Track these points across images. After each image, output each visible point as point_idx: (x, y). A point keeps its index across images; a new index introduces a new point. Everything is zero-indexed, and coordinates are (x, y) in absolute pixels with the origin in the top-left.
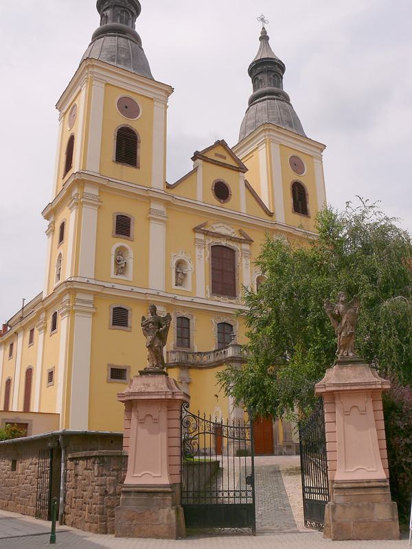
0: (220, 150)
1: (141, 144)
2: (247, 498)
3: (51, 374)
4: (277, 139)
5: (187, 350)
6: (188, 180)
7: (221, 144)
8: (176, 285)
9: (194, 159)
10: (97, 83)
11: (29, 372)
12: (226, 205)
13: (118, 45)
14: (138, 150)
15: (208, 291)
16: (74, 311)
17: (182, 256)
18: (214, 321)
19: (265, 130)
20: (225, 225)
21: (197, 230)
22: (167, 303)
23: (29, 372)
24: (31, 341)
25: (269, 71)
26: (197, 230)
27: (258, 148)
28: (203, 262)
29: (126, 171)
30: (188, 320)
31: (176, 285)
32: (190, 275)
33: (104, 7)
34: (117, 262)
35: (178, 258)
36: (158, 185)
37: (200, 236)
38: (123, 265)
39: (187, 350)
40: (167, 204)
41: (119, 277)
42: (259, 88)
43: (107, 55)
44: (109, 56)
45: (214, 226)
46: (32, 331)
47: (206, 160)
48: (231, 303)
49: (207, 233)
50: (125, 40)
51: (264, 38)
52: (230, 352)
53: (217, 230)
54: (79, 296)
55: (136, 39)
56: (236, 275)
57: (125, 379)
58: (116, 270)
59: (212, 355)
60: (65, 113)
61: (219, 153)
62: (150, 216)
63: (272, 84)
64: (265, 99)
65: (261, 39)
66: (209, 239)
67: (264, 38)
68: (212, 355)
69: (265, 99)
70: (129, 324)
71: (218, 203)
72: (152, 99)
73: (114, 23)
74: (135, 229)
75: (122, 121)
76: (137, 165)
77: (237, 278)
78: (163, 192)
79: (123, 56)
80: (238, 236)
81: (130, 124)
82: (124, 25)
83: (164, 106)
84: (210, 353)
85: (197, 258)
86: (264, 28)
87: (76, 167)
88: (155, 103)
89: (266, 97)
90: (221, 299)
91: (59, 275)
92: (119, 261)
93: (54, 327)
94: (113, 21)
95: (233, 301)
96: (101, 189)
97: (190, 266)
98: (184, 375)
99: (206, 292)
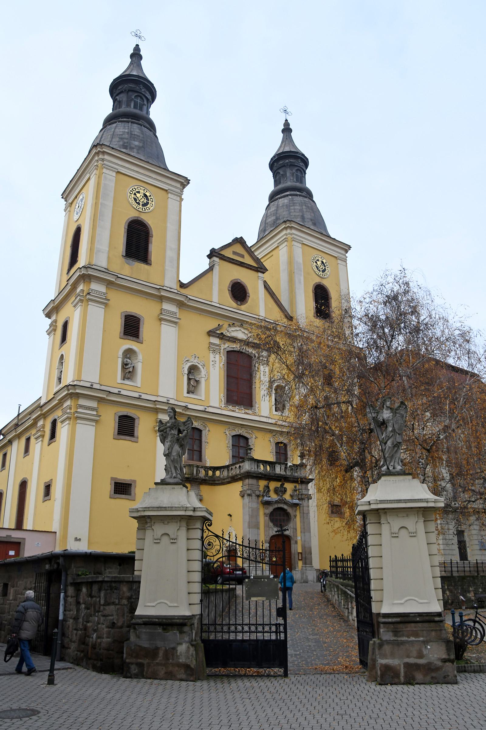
0: (238, 248)
1: (153, 238)
2: (229, 633)
3: (48, 488)
5: (198, 463)
6: (203, 279)
7: (240, 241)
9: (210, 256)
11: (23, 485)
12: (243, 307)
14: (150, 245)
15: (223, 400)
17: (195, 362)
21: (211, 333)
23: (23, 485)
24: (27, 450)
25: (292, 165)
26: (211, 333)
27: (278, 247)
28: (217, 365)
31: (188, 393)
33: (118, 92)
34: (125, 365)
35: (192, 363)
36: (170, 283)
37: (216, 341)
38: (131, 370)
39: (198, 463)
41: (127, 382)
44: (121, 143)
46: (28, 440)
48: (247, 414)
49: (222, 337)
50: (139, 126)
53: (234, 334)
54: (82, 402)
61: (238, 251)
63: (295, 180)
64: (287, 195)
66: (224, 344)
69: (287, 195)
70: (136, 434)
71: (234, 304)
72: (166, 191)
74: (145, 330)
76: (149, 262)
77: (254, 387)
78: (176, 291)
79: (137, 143)
82: (137, 111)
84: (224, 467)
85: (212, 363)
86: (286, 120)
87: (82, 261)
88: (170, 195)
89: (288, 193)
90: (236, 408)
91: (60, 379)
92: (126, 365)
93: (53, 435)
95: (250, 412)
96: (108, 286)
97: (203, 372)
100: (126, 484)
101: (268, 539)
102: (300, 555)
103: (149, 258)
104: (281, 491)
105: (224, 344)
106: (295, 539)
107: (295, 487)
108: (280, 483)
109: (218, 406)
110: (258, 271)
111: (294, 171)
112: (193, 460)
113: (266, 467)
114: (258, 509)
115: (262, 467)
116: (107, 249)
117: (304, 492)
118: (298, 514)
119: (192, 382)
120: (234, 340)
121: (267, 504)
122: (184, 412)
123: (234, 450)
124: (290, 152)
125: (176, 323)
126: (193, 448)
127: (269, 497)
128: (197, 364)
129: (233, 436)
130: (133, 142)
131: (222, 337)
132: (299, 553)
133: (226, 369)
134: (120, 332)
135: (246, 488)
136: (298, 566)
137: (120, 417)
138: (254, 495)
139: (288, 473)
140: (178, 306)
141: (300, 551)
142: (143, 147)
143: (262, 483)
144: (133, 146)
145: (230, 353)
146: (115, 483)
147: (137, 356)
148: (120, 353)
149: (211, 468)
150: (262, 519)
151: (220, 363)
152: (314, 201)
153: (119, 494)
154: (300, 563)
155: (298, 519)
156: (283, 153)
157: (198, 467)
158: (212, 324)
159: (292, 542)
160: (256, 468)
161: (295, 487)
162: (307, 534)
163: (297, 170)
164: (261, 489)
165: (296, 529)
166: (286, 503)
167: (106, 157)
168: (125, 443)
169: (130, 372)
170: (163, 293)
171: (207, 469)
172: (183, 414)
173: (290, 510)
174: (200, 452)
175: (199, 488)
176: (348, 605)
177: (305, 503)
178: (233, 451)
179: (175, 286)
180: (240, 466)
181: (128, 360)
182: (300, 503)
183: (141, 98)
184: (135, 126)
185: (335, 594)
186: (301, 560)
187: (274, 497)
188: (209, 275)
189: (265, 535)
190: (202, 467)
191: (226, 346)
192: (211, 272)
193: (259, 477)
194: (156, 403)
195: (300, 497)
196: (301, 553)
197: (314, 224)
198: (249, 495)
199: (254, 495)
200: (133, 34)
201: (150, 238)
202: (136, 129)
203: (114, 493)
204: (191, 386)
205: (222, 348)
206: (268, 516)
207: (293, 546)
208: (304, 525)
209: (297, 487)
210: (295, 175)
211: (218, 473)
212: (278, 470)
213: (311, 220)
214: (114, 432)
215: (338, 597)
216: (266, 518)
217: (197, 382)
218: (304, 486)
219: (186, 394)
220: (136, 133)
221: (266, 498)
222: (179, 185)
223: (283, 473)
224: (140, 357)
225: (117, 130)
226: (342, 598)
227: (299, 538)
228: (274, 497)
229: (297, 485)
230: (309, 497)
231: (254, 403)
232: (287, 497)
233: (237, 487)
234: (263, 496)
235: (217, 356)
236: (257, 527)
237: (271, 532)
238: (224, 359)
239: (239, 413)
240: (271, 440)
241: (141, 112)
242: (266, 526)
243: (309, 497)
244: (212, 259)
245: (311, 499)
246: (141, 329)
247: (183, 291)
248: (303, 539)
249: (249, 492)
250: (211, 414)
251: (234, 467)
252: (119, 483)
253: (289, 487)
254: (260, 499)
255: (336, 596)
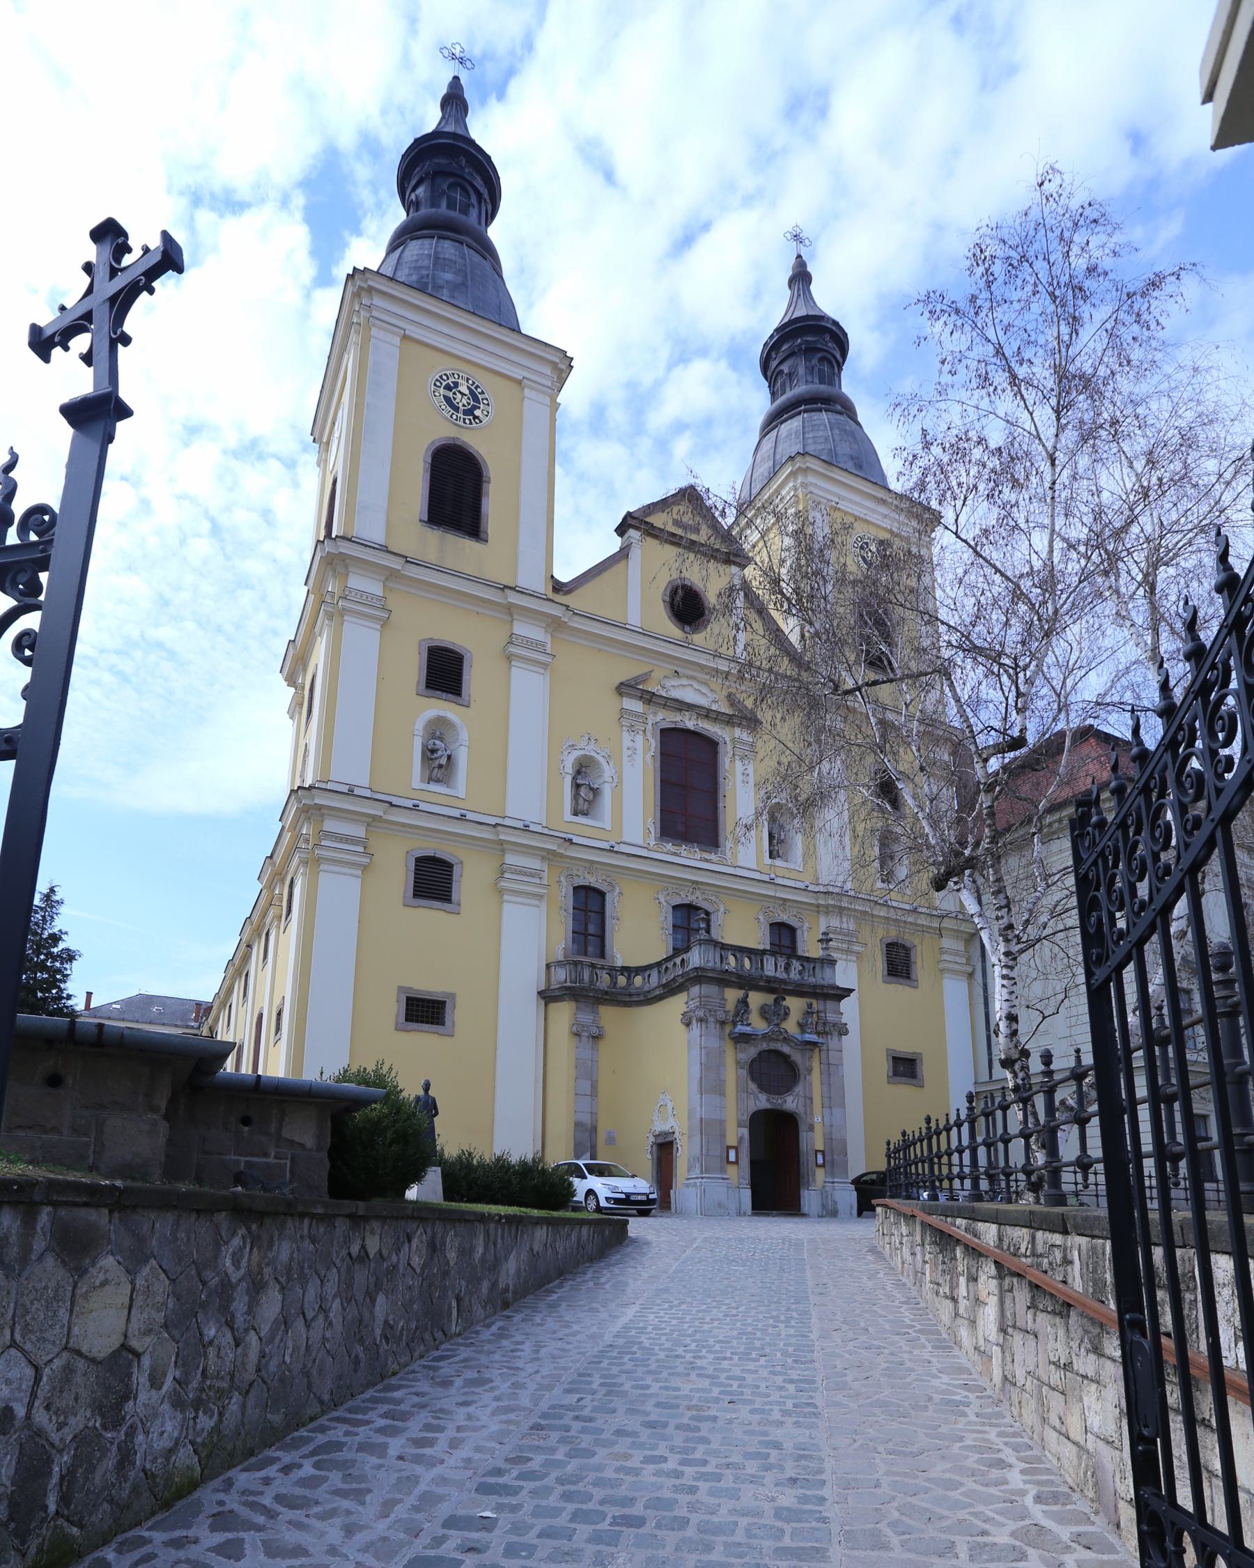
0: (683, 511)
4: (822, 494)
5: (600, 962)
6: (606, 576)
7: (690, 496)
8: (576, 814)
9: (621, 530)
10: (382, 335)
12: (698, 638)
13: (436, 252)
14: (484, 500)
15: (652, 830)
16: (319, 860)
17: (590, 750)
18: (668, 900)
19: (793, 474)
20: (696, 685)
21: (625, 689)
22: (549, 851)
25: (809, 351)
26: (625, 689)
28: (639, 758)
29: (459, 549)
30: (602, 894)
32: (607, 791)
33: (413, 182)
34: (429, 753)
35: (582, 752)
36: (529, 577)
37: (636, 706)
38: (443, 761)
39: (600, 962)
40: (555, 625)
41: (433, 787)
42: (783, 393)
43: (411, 275)
45: (668, 683)
47: (651, 532)
48: (707, 861)
49: (649, 698)
51: (801, 278)
52: (695, 958)
53: (675, 694)
54: (330, 825)
55: (487, 251)
56: (721, 796)
57: (443, 1024)
58: (427, 772)
59: (654, 973)
60: (328, 443)
62: (512, 649)
63: (817, 380)
64: (799, 413)
65: (792, 282)
66: (655, 714)
67: (801, 278)
68: (654, 973)
70: (454, 897)
71: (673, 630)
72: (519, 382)
73: (433, 210)
74: (475, 678)
75: (443, 429)
76: (482, 535)
77: (721, 805)
79: (449, 276)
80: (725, 708)
81: (465, 439)
82: (455, 214)
83: (547, 400)
84: (649, 967)
85: (626, 753)
86: (799, 256)
90: (683, 849)
92: (433, 751)
94: (433, 206)
95: (713, 857)
96: (391, 584)
97: (608, 771)
98: (586, 1017)
99: (814, 1174)
100: (434, 1002)
101: (746, 1118)
102: (820, 1157)
103: (482, 529)
104: (774, 1014)
105: (655, 714)
106: (809, 1121)
107: (810, 1006)
108: (774, 996)
109: (641, 843)
110: (728, 562)
111: (814, 361)
112: (586, 954)
113: (742, 961)
114: (722, 1052)
115: (732, 960)
116: (386, 505)
117: (831, 1017)
118: (815, 1064)
119: (583, 792)
120: (681, 706)
121: (742, 1039)
122: (562, 851)
123: (679, 937)
124: (807, 318)
125: (545, 666)
126: (586, 929)
127: (749, 1025)
128: (593, 754)
129: (675, 908)
130: (442, 274)
131: (649, 698)
132: (817, 1151)
133: (658, 765)
134: (418, 682)
135: (692, 1005)
136: (814, 1180)
137: (419, 860)
138: (711, 1019)
139: (792, 976)
140: (550, 630)
141: (819, 1146)
142: (464, 284)
143: (732, 995)
144: (441, 282)
145: (667, 734)
146: (408, 999)
147: (458, 734)
148: (419, 726)
149: (625, 970)
150: (732, 1075)
151: (645, 753)
152: (858, 424)
153: (417, 1021)
154: (820, 1174)
155: (816, 1078)
156: (791, 322)
157: (593, 966)
158: (627, 671)
159: (802, 1127)
160: (718, 960)
161: (810, 1006)
162: (836, 1111)
163: (821, 360)
164: (731, 1006)
165: (811, 1099)
166: (787, 1039)
167: (378, 301)
168: (429, 915)
169: (440, 766)
170: (513, 598)
171: (613, 971)
172: (562, 856)
173: (796, 1057)
174: (602, 937)
175: (595, 1012)
176: (954, 1286)
177: (833, 1042)
178: (674, 939)
179: (542, 587)
180: (683, 960)
181: (437, 742)
182: (821, 1040)
183: (464, 189)
184: (447, 244)
185: (901, 1243)
186: (823, 1166)
187: (758, 1025)
188: (620, 566)
189: (738, 1110)
190: (602, 968)
191: (660, 716)
192: (623, 563)
193: (724, 980)
194: (499, 828)
195: (820, 1028)
196: (823, 1152)
197: (860, 467)
198: (701, 1020)
199: (711, 1019)
200: (446, 52)
201: (485, 485)
202: (448, 249)
203: (407, 1020)
204: (581, 801)
205: (650, 722)
206: (747, 1067)
207: (804, 1136)
208: (829, 1091)
209: (815, 1005)
210: (816, 369)
211: (638, 980)
212: (770, 968)
213: (852, 458)
214: (405, 892)
215: (913, 1254)
216: (740, 1071)
217: (596, 792)
218: (830, 1005)
219: (568, 817)
220: (447, 256)
221: (740, 1028)
222: (547, 370)
223: (781, 974)
224: (464, 735)
225: (407, 253)
226: (927, 1257)
227: (818, 1119)
228: (758, 1025)
229: (815, 1003)
230: (843, 1030)
231: (721, 839)
232: (790, 1026)
233: (677, 1005)
234: (734, 1023)
235: (639, 738)
236: (720, 1091)
237: (751, 1102)
238: (653, 745)
239: (690, 856)
240: (761, 917)
241: (463, 217)
242: (741, 1089)
243: (843, 1030)
244: (626, 536)
245: (846, 1033)
246: (464, 677)
247: (559, 598)
248: (827, 1123)
249: (700, 1013)
250: (624, 857)
251: (670, 965)
252: (418, 1000)
253: (795, 1005)
254: (728, 1029)
255: (906, 1251)
